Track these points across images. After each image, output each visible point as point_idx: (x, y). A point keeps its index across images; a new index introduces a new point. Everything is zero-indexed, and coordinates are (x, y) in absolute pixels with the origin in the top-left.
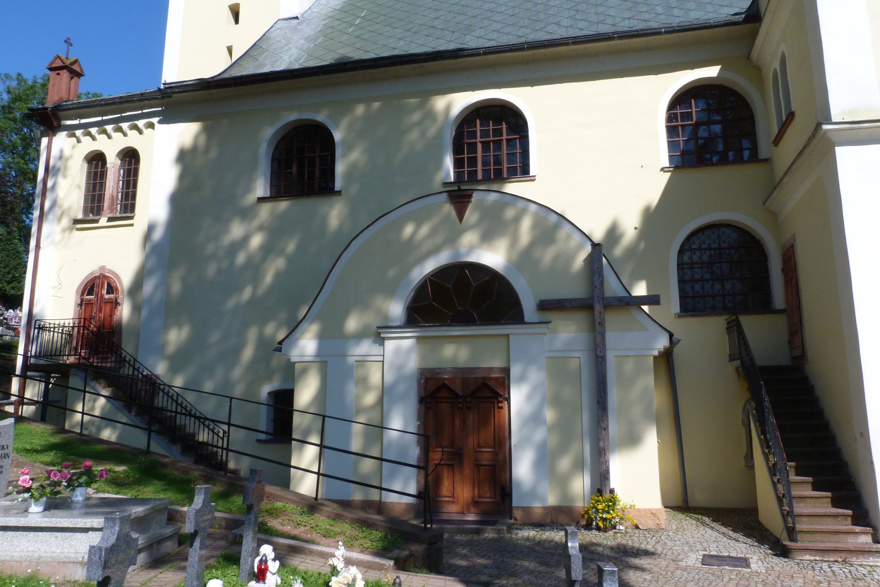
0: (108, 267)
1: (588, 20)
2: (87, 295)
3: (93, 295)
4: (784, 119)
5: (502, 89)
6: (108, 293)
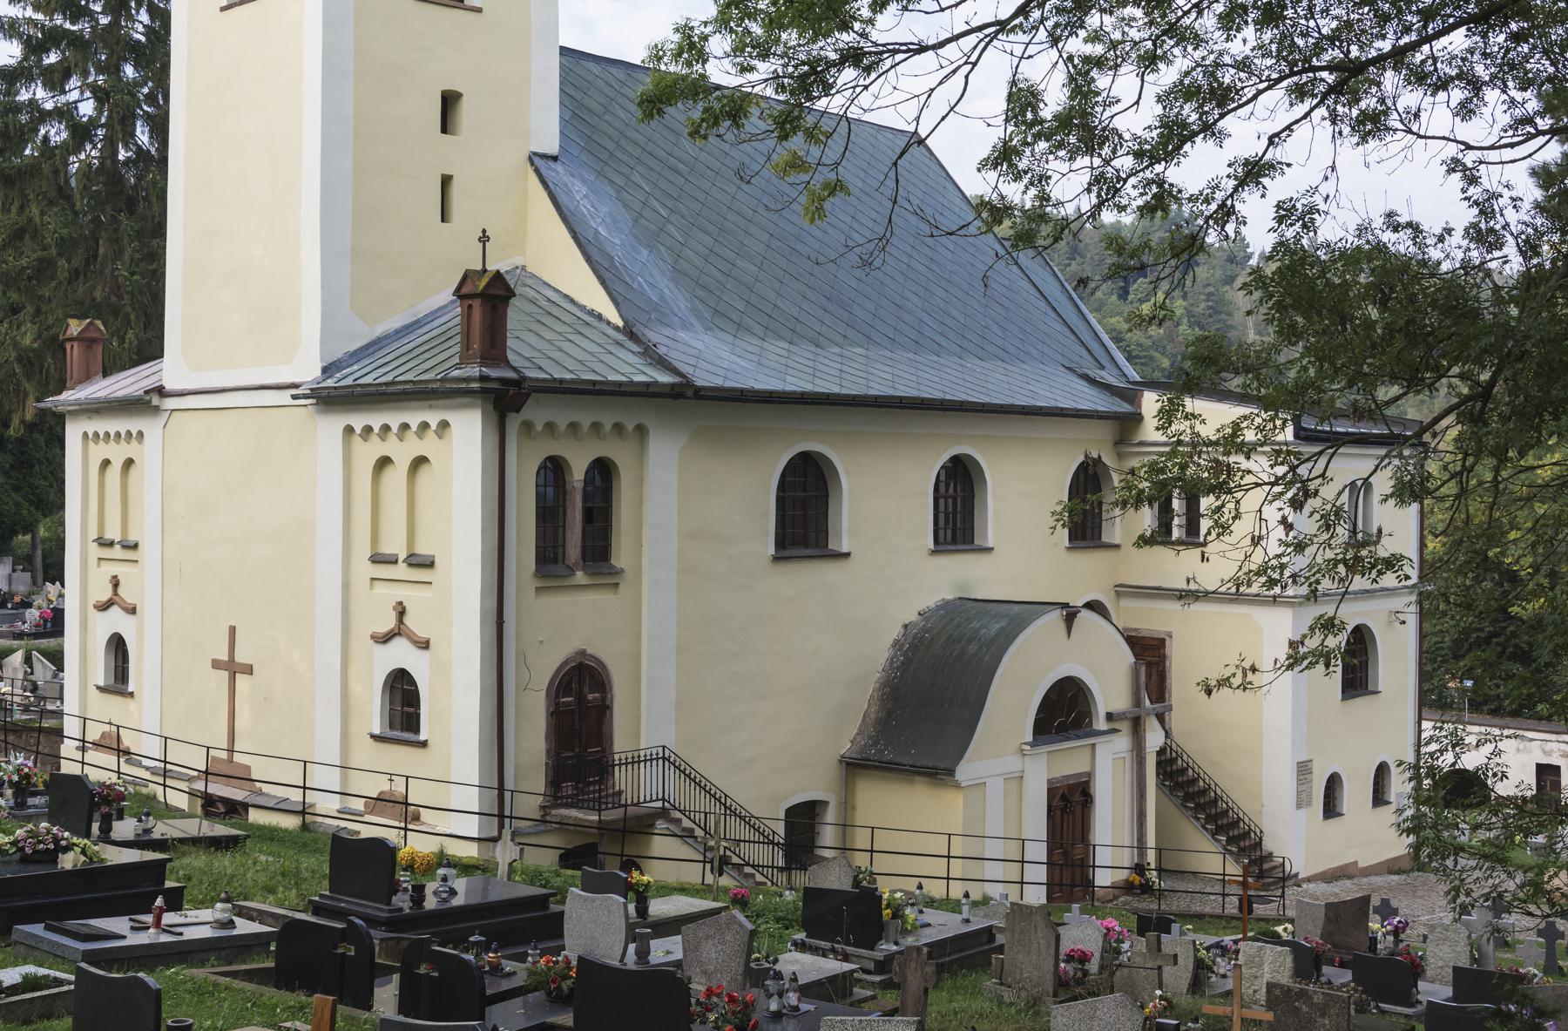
0: (590, 651)
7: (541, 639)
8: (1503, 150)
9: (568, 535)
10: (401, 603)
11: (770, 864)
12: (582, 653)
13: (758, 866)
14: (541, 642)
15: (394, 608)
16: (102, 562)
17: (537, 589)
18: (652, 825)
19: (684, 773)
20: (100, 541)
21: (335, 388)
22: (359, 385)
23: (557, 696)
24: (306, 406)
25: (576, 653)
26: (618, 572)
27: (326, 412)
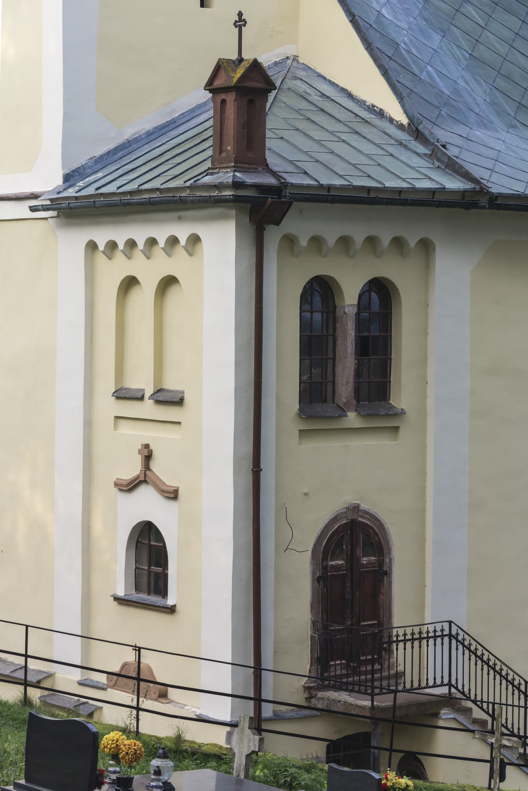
0: (364, 506)
7: (305, 491)
9: (339, 369)
10: (147, 446)
12: (356, 508)
14: (306, 494)
15: (140, 452)
16: (122, 422)
18: (436, 715)
20: (161, 397)
21: (76, 198)
22: (102, 194)
23: (325, 558)
24: (46, 219)
25: (348, 508)
26: (399, 414)
27: (68, 225)
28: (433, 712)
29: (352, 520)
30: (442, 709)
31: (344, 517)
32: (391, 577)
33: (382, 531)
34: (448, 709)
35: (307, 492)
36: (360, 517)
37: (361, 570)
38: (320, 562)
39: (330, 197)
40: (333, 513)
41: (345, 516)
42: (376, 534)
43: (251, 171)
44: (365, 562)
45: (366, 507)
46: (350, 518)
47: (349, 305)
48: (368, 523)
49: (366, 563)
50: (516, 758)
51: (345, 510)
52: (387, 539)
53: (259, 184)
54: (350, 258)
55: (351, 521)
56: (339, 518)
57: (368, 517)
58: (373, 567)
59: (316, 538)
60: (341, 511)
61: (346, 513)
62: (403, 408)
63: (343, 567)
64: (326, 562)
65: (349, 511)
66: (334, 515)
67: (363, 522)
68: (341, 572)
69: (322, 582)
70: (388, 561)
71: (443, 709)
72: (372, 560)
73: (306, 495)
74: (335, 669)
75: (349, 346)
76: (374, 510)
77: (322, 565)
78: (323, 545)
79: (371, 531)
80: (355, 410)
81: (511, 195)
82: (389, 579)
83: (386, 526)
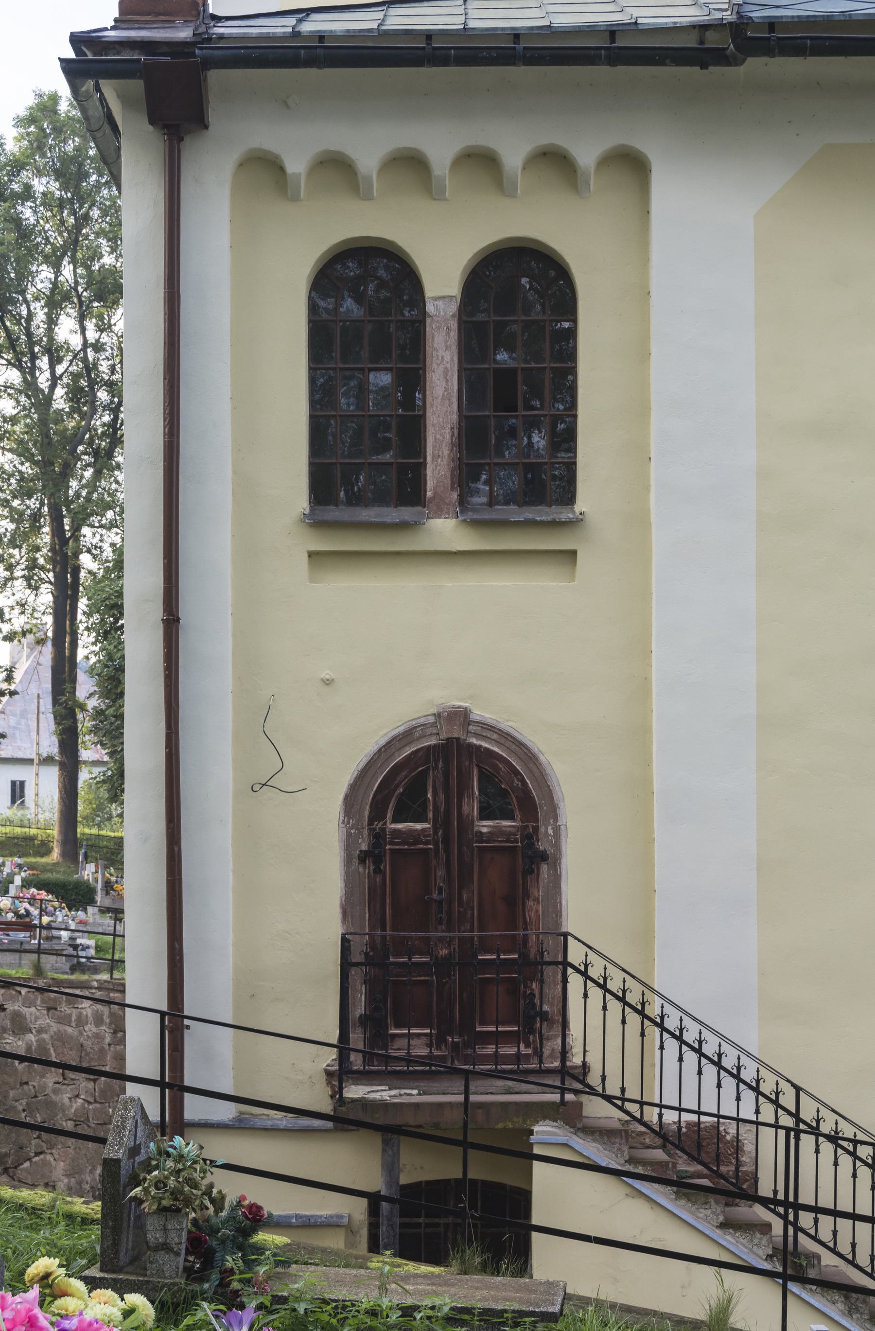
0: (479, 713)
1: (64, 953)
2: (395, 821)
3: (423, 820)
4: (700, 1167)
5: (849, 58)
6: (485, 814)
7: (325, 674)
8: (23, 954)
11: (781, 1196)
12: (461, 716)
13: (777, 1203)
14: (328, 682)
17: (311, 555)
19: (661, 1026)
23: (378, 811)
25: (438, 716)
28: (511, 1126)
29: (448, 739)
30: (537, 1122)
31: (431, 735)
32: (560, 865)
33: (535, 770)
34: (555, 1124)
35: (328, 677)
36: (473, 737)
37: (475, 845)
38: (366, 823)
39: (303, 52)
40: (400, 724)
41: (435, 731)
42: (516, 772)
43: (155, 26)
44: (485, 830)
45: (487, 716)
46: (444, 735)
47: (436, 299)
48: (496, 749)
49: (489, 832)
50: (764, 1257)
51: (431, 719)
52: (548, 786)
53: (139, 39)
54: (435, 199)
55: (447, 743)
56: (417, 734)
57: (495, 736)
58: (508, 841)
59: (356, 773)
60: (422, 721)
61: (433, 725)
62: (584, 510)
63: (428, 836)
64: (381, 823)
65: (440, 723)
66: (401, 729)
67: (481, 746)
68: (421, 846)
69: (372, 864)
70: (550, 831)
71: (541, 1123)
72: (505, 827)
73: (327, 684)
74: (409, 1045)
75: (438, 382)
76: (510, 724)
77: (370, 829)
78: (375, 789)
79: (501, 766)
80: (455, 515)
81: (804, 20)
82: (556, 870)
83: (542, 758)
